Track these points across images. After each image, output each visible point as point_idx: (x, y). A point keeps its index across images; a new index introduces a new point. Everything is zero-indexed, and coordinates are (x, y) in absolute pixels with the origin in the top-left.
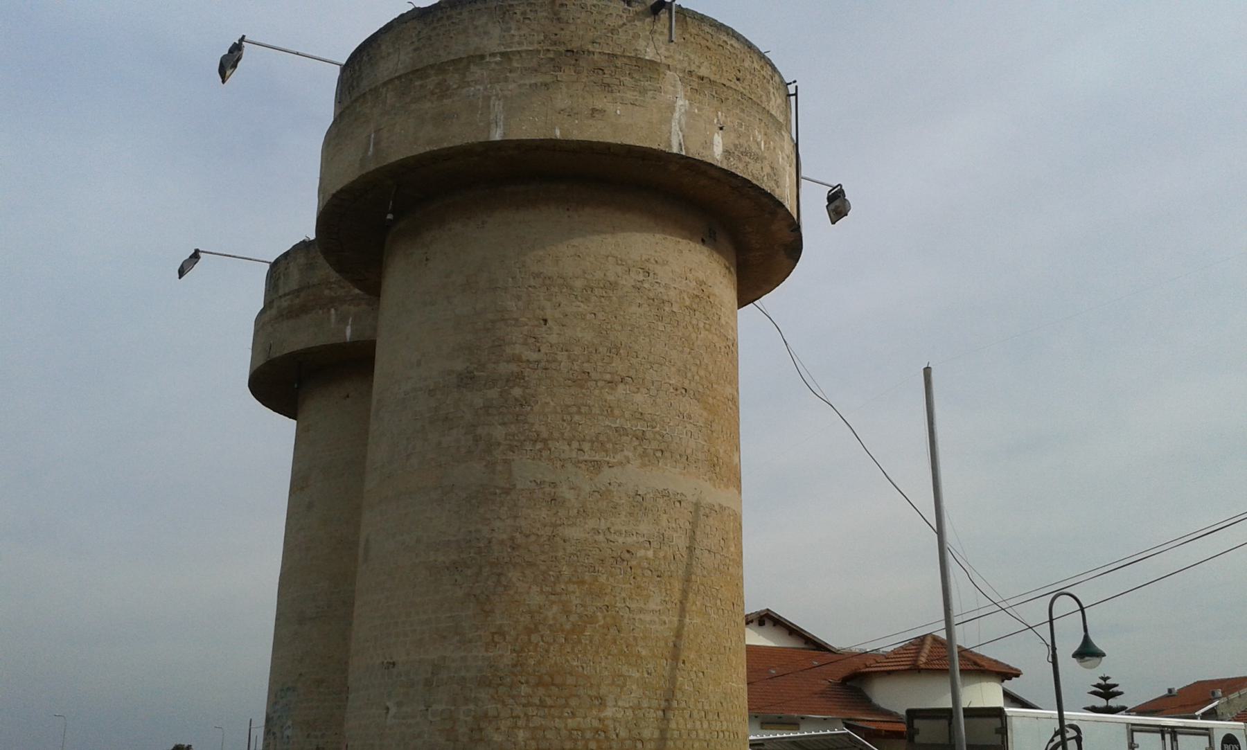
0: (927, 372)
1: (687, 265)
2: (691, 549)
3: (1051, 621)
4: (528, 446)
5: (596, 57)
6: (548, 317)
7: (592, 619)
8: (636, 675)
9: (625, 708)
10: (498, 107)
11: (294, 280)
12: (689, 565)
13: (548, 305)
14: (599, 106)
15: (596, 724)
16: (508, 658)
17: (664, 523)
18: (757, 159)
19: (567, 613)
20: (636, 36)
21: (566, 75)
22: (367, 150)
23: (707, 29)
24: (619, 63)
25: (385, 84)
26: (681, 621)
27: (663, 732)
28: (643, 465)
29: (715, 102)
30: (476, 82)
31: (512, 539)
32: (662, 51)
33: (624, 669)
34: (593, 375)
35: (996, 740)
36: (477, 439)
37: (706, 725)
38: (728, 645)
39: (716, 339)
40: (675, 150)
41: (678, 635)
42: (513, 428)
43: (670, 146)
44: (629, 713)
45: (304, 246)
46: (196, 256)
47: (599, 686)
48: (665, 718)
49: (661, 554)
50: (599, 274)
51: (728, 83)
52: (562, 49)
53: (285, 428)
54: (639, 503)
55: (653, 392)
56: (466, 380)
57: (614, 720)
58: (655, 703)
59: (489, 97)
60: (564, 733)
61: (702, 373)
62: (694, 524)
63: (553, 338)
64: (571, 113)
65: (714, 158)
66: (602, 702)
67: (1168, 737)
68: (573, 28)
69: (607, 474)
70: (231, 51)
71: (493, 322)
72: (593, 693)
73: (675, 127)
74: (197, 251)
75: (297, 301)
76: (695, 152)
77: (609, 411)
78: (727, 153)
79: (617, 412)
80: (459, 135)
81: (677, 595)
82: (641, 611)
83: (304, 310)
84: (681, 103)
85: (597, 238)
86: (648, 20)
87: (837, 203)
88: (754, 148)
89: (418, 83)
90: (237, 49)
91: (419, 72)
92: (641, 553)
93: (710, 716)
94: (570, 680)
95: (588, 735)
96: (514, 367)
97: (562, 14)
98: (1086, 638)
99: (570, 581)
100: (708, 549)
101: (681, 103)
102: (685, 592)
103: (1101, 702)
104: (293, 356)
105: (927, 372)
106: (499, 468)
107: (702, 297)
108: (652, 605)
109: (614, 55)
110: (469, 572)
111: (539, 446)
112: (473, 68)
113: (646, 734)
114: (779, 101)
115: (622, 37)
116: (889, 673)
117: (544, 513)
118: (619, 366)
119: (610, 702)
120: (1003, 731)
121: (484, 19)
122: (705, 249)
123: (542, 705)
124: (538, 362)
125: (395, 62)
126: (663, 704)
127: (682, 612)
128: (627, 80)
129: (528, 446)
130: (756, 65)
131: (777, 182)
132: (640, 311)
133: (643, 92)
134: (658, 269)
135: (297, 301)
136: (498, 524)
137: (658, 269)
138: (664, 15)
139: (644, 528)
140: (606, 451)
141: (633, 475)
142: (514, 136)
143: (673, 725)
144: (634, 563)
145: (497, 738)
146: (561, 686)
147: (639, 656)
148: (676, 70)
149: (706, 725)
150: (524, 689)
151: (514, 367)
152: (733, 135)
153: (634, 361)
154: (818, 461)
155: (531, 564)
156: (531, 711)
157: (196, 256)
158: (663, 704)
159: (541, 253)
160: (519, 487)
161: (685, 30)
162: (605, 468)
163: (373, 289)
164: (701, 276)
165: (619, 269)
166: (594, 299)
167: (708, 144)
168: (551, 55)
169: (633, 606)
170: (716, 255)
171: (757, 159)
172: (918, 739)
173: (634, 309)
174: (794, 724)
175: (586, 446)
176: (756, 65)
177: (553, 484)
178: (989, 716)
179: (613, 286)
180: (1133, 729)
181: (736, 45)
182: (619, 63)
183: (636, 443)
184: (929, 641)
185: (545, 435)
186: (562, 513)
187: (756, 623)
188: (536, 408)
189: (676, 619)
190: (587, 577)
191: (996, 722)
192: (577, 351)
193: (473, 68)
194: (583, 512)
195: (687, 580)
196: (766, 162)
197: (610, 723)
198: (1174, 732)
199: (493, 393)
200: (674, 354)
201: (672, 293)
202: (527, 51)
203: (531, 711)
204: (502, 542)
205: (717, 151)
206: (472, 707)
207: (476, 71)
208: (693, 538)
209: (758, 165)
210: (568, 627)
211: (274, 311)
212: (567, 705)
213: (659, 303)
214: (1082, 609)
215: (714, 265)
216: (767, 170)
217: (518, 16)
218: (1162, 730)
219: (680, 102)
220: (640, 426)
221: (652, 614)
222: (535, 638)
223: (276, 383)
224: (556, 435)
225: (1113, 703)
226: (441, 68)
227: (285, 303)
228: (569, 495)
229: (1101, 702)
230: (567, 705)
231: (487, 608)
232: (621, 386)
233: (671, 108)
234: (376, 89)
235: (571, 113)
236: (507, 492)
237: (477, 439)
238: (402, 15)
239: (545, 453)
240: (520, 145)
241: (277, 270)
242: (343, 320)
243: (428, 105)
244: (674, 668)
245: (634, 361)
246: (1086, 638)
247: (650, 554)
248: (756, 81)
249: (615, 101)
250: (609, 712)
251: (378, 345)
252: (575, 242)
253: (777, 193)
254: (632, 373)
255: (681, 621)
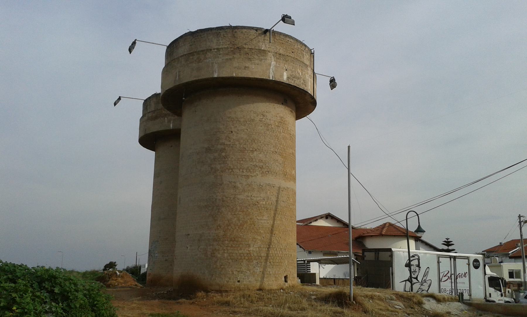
0: (349, 147)
1: (277, 112)
2: (277, 201)
3: (407, 219)
4: (227, 171)
5: (246, 50)
6: (233, 131)
7: (246, 222)
8: (259, 238)
9: (256, 248)
10: (216, 66)
11: (152, 107)
12: (276, 206)
13: (233, 127)
14: (247, 65)
15: (247, 252)
16: (222, 233)
17: (269, 193)
18: (298, 78)
19: (239, 220)
20: (259, 42)
21: (237, 56)
22: (176, 77)
23: (282, 37)
24: (253, 51)
25: (181, 56)
26: (274, 222)
27: (267, 254)
28: (262, 176)
29: (284, 62)
30: (209, 58)
31: (223, 199)
32: (267, 46)
33: (256, 237)
34: (247, 149)
35: (389, 259)
36: (212, 169)
37: (281, 252)
38: (289, 229)
39: (286, 135)
40: (271, 79)
41: (273, 226)
42: (222, 165)
43: (269, 78)
44: (257, 249)
45: (156, 95)
46: (119, 99)
47: (248, 241)
48: (268, 250)
49: (268, 203)
50: (248, 117)
51: (289, 55)
52: (236, 47)
53: (151, 155)
54: (261, 188)
55: (265, 153)
56: (208, 150)
57: (253, 251)
58: (265, 246)
59: (213, 63)
60: (238, 254)
61: (281, 146)
62: (278, 194)
63: (234, 138)
64: (239, 68)
65: (283, 80)
66: (249, 246)
67: (452, 259)
68: (239, 39)
69: (250, 180)
70: (132, 44)
71: (216, 132)
72: (247, 243)
73: (271, 70)
74: (120, 97)
75: (154, 115)
76: (278, 79)
77: (252, 160)
78: (288, 78)
79: (254, 160)
80: (204, 75)
81: (272, 215)
82: (261, 220)
83: (156, 118)
84: (273, 63)
85: (248, 105)
86: (263, 36)
87: (332, 83)
88: (297, 75)
89: (191, 57)
90: (134, 43)
91: (192, 54)
92: (261, 203)
93: (282, 250)
94: (240, 240)
95: (245, 255)
96: (223, 147)
97: (236, 35)
98: (419, 226)
99: (240, 211)
100: (285, 199)
101: (273, 63)
102: (275, 214)
103: (446, 247)
104: (153, 133)
105: (349, 147)
106: (218, 177)
107: (282, 122)
108: (265, 218)
109: (252, 49)
110: (210, 208)
111: (230, 171)
112: (208, 53)
113: (262, 255)
114: (308, 56)
115: (254, 42)
116: (372, 236)
117: (232, 191)
118: (255, 146)
119: (252, 246)
120: (391, 256)
121: (211, 36)
122: (283, 106)
123: (232, 246)
124: (230, 145)
125: (183, 50)
126: (268, 246)
127: (274, 220)
128: (256, 57)
129: (227, 171)
130: (299, 47)
131: (305, 85)
132: (261, 128)
133: (261, 60)
134: (267, 114)
135: (154, 115)
136: (218, 194)
137: (267, 114)
138: (268, 34)
139: (263, 195)
140: (251, 172)
141: (259, 179)
142: (221, 76)
143: (270, 252)
144: (259, 206)
145: (219, 256)
146: (237, 241)
147: (260, 233)
148: (271, 52)
149: (281, 252)
150: (226, 242)
151: (223, 147)
152: (290, 72)
153: (259, 144)
154: (336, 165)
155: (228, 206)
156: (229, 248)
157: (119, 99)
158: (268, 246)
159: (230, 110)
160: (224, 183)
161: (275, 38)
162: (250, 177)
163: (180, 115)
164: (282, 115)
165: (255, 115)
166: (247, 125)
167: (282, 76)
168: (232, 49)
169: (259, 218)
170: (287, 108)
171: (298, 78)
172: (365, 259)
173: (260, 127)
174: (336, 254)
175: (245, 171)
176: (299, 47)
177: (235, 182)
178: (387, 251)
179: (253, 120)
180: (439, 257)
181: (292, 41)
182: (253, 51)
183: (260, 169)
184: (387, 225)
185: (232, 167)
186: (237, 191)
187: (324, 218)
188: (229, 159)
189: (272, 222)
190: (245, 210)
191: (389, 253)
192: (242, 141)
193: (208, 53)
194: (244, 191)
195: (276, 210)
196: (302, 79)
197: (251, 252)
198: (455, 258)
199: (216, 155)
200: (272, 141)
201: (272, 122)
202: (225, 48)
203: (229, 248)
204: (220, 200)
205: (285, 78)
206: (211, 247)
207: (209, 54)
208: (278, 198)
209: (299, 81)
210: (239, 224)
211: (146, 118)
212: (239, 247)
213: (267, 125)
214: (418, 215)
215: (286, 111)
216: (302, 81)
217: (222, 36)
218: (450, 257)
219: (273, 63)
220: (261, 164)
221: (264, 221)
222: (229, 228)
223: (148, 140)
224: (235, 167)
225: (450, 248)
226: (198, 53)
227: (150, 115)
228: (239, 186)
229: (446, 247)
230: (239, 247)
231: (216, 219)
232: (255, 152)
233: (270, 65)
234: (178, 58)
235: (239, 68)
236: (221, 185)
237: (212, 169)
238: (186, 33)
239: (232, 173)
240: (223, 78)
241: (147, 103)
242: (169, 122)
243: (194, 65)
244: (271, 236)
245: (259, 144)
246: (419, 226)
247: (264, 203)
248: (299, 52)
249: (252, 64)
250: (251, 249)
251: (182, 130)
252: (241, 107)
253: (305, 89)
254: (259, 148)
255: (274, 222)
